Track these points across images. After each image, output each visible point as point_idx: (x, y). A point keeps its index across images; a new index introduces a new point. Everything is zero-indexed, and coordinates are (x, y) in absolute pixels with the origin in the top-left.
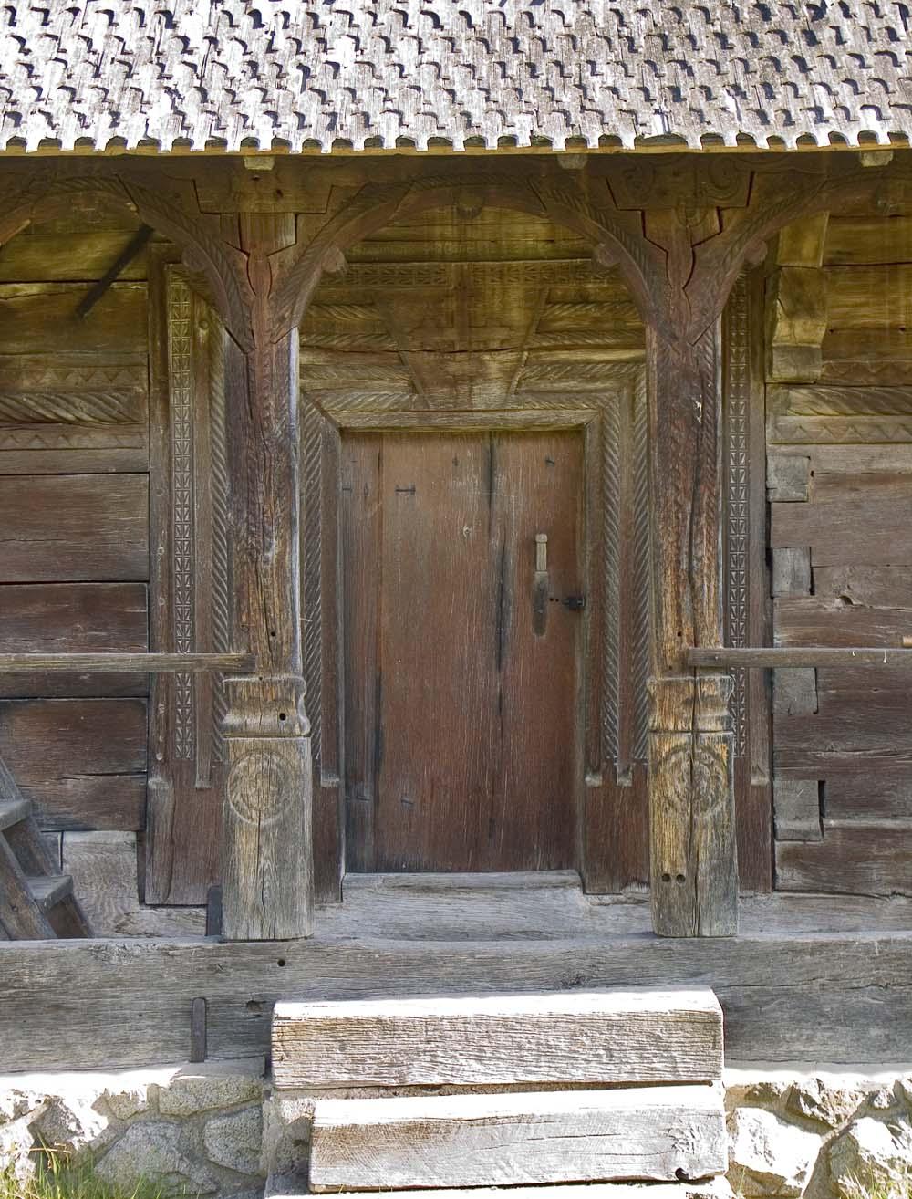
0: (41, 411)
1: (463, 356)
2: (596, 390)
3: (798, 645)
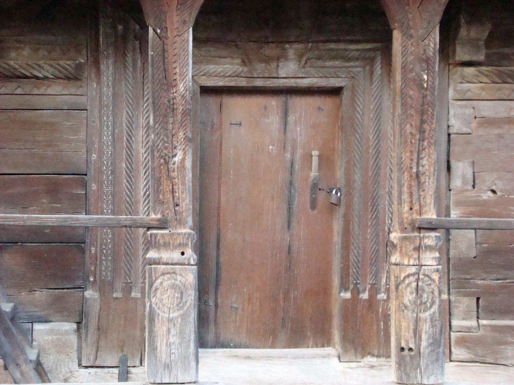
0: (23, 71)
2: (350, 67)
3: (465, 217)
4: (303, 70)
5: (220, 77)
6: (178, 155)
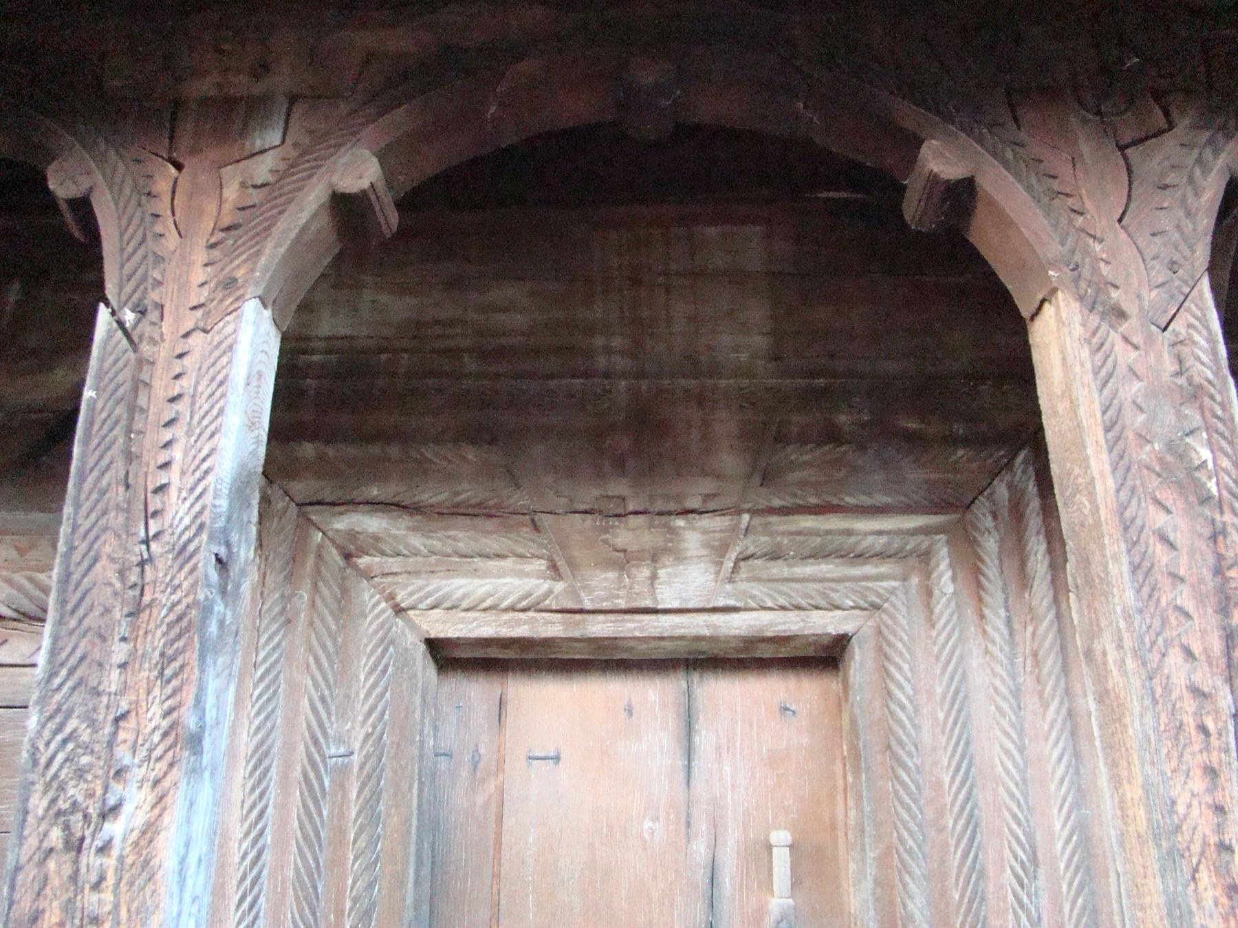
1: (641, 519)
2: (866, 578)
4: (728, 587)
5: (485, 610)
6: (127, 809)
